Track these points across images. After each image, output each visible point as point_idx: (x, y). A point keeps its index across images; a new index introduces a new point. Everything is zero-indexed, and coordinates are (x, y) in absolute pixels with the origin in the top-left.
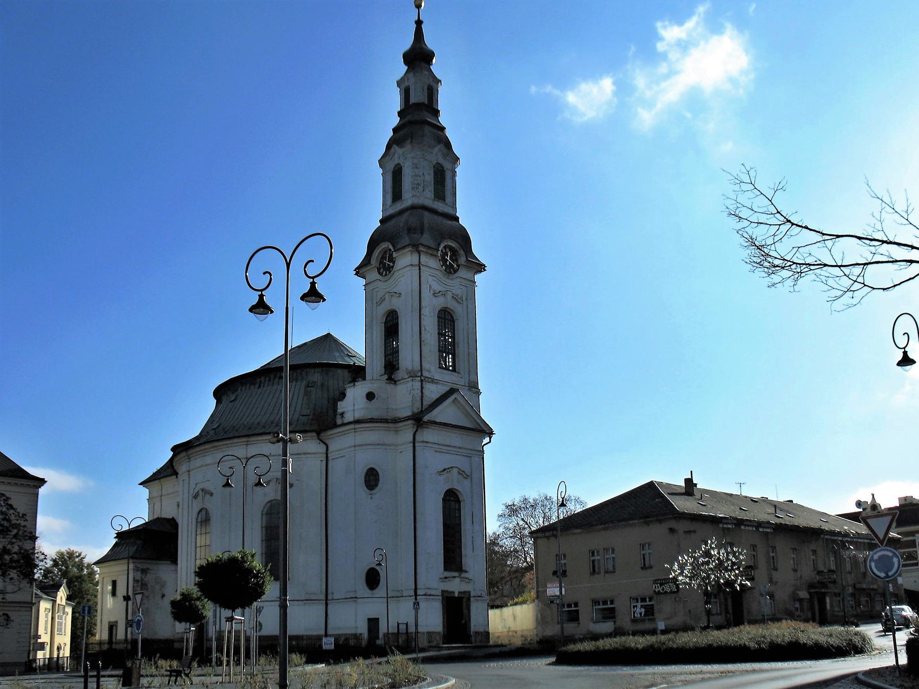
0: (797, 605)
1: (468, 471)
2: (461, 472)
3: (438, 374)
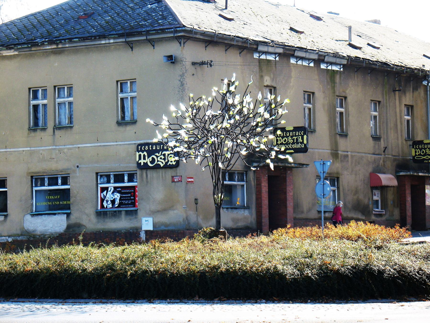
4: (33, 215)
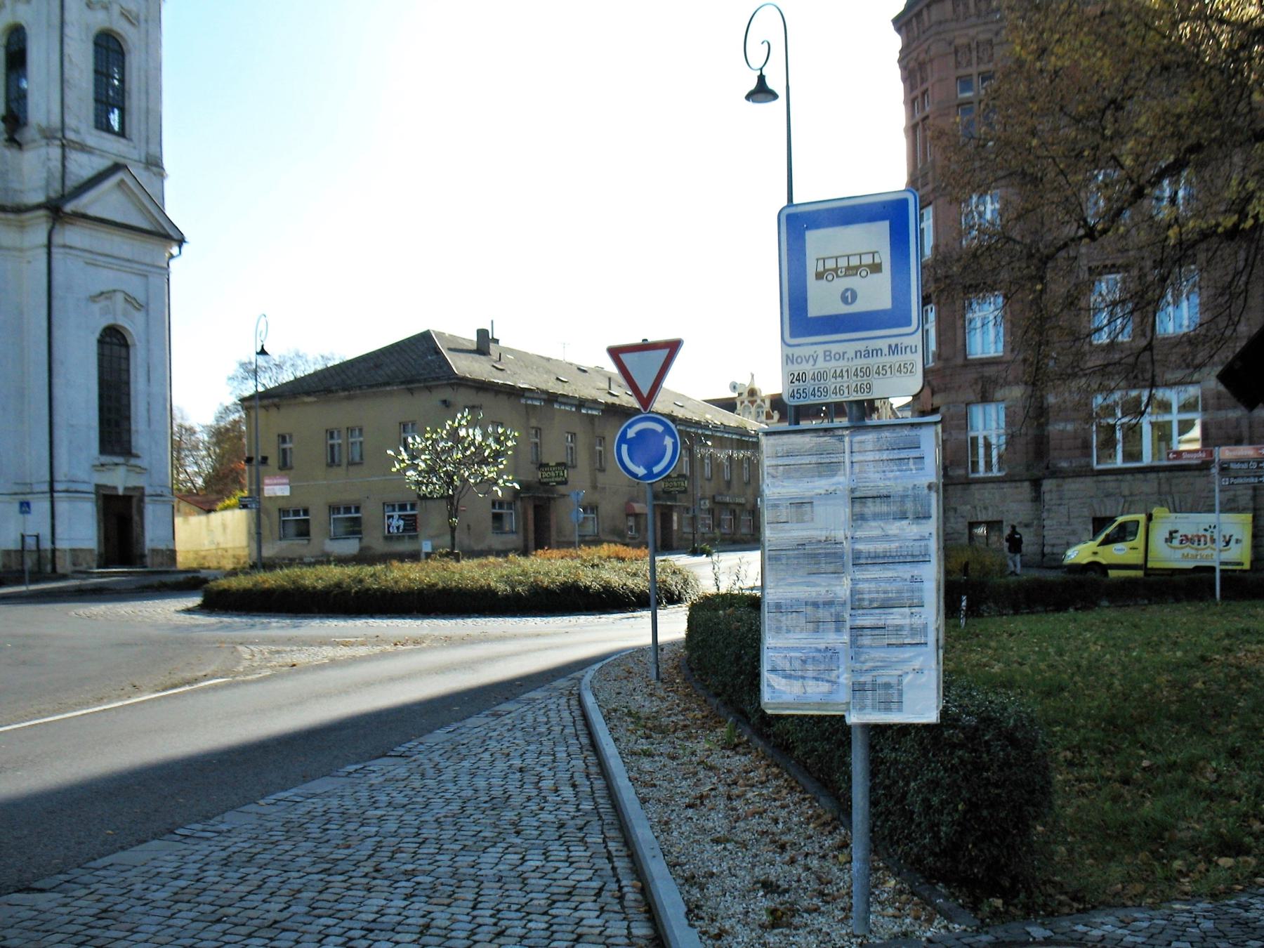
0: (631, 522)
1: (141, 297)
2: (130, 299)
3: (94, 138)
4: (331, 539)
